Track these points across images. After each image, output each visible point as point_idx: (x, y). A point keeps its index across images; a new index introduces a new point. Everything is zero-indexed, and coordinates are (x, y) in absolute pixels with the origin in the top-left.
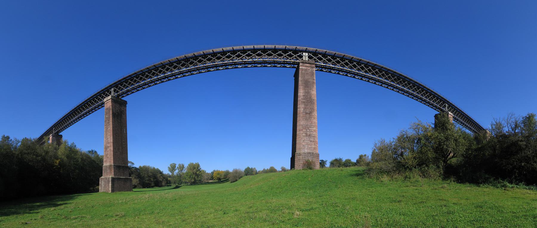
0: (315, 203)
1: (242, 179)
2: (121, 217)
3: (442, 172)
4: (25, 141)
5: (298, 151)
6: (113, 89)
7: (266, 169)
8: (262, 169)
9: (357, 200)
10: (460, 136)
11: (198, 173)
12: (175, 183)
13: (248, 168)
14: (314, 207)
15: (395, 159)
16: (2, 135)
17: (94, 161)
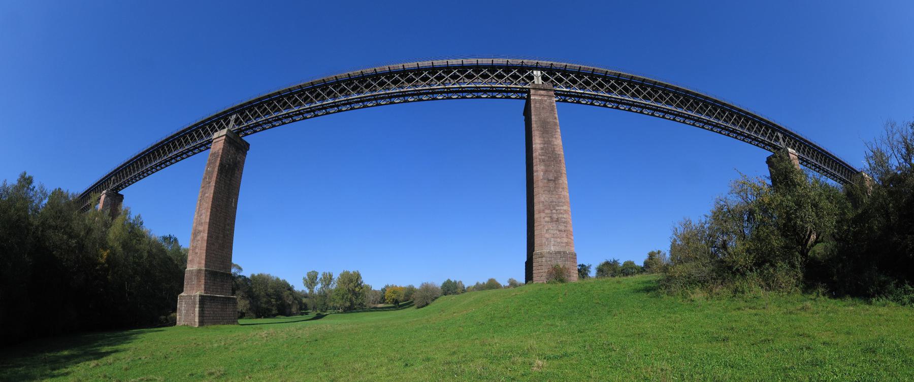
0: (571, 344)
1: (437, 301)
2: (219, 377)
3: (800, 275)
4: (58, 194)
5: (537, 250)
6: (234, 117)
7: (481, 283)
8: (473, 284)
9: (648, 338)
10: (820, 195)
11: (357, 289)
12: (314, 308)
13: (449, 282)
14: (569, 351)
15: (713, 256)
16: (21, 172)
17: (170, 259)
